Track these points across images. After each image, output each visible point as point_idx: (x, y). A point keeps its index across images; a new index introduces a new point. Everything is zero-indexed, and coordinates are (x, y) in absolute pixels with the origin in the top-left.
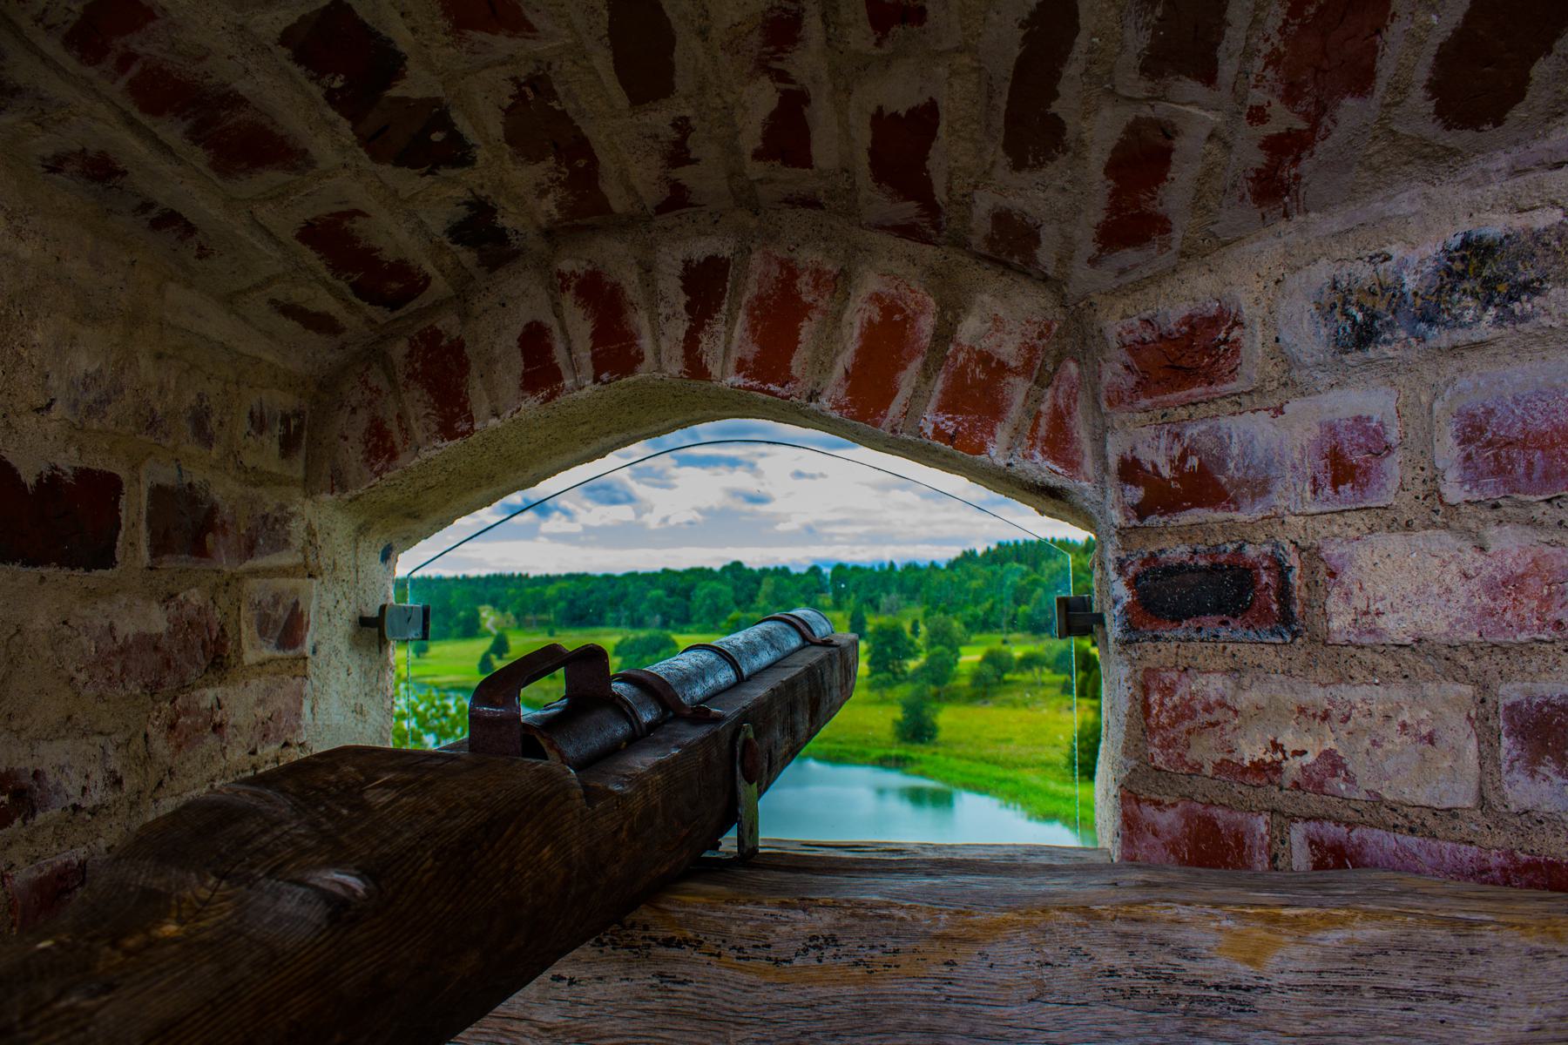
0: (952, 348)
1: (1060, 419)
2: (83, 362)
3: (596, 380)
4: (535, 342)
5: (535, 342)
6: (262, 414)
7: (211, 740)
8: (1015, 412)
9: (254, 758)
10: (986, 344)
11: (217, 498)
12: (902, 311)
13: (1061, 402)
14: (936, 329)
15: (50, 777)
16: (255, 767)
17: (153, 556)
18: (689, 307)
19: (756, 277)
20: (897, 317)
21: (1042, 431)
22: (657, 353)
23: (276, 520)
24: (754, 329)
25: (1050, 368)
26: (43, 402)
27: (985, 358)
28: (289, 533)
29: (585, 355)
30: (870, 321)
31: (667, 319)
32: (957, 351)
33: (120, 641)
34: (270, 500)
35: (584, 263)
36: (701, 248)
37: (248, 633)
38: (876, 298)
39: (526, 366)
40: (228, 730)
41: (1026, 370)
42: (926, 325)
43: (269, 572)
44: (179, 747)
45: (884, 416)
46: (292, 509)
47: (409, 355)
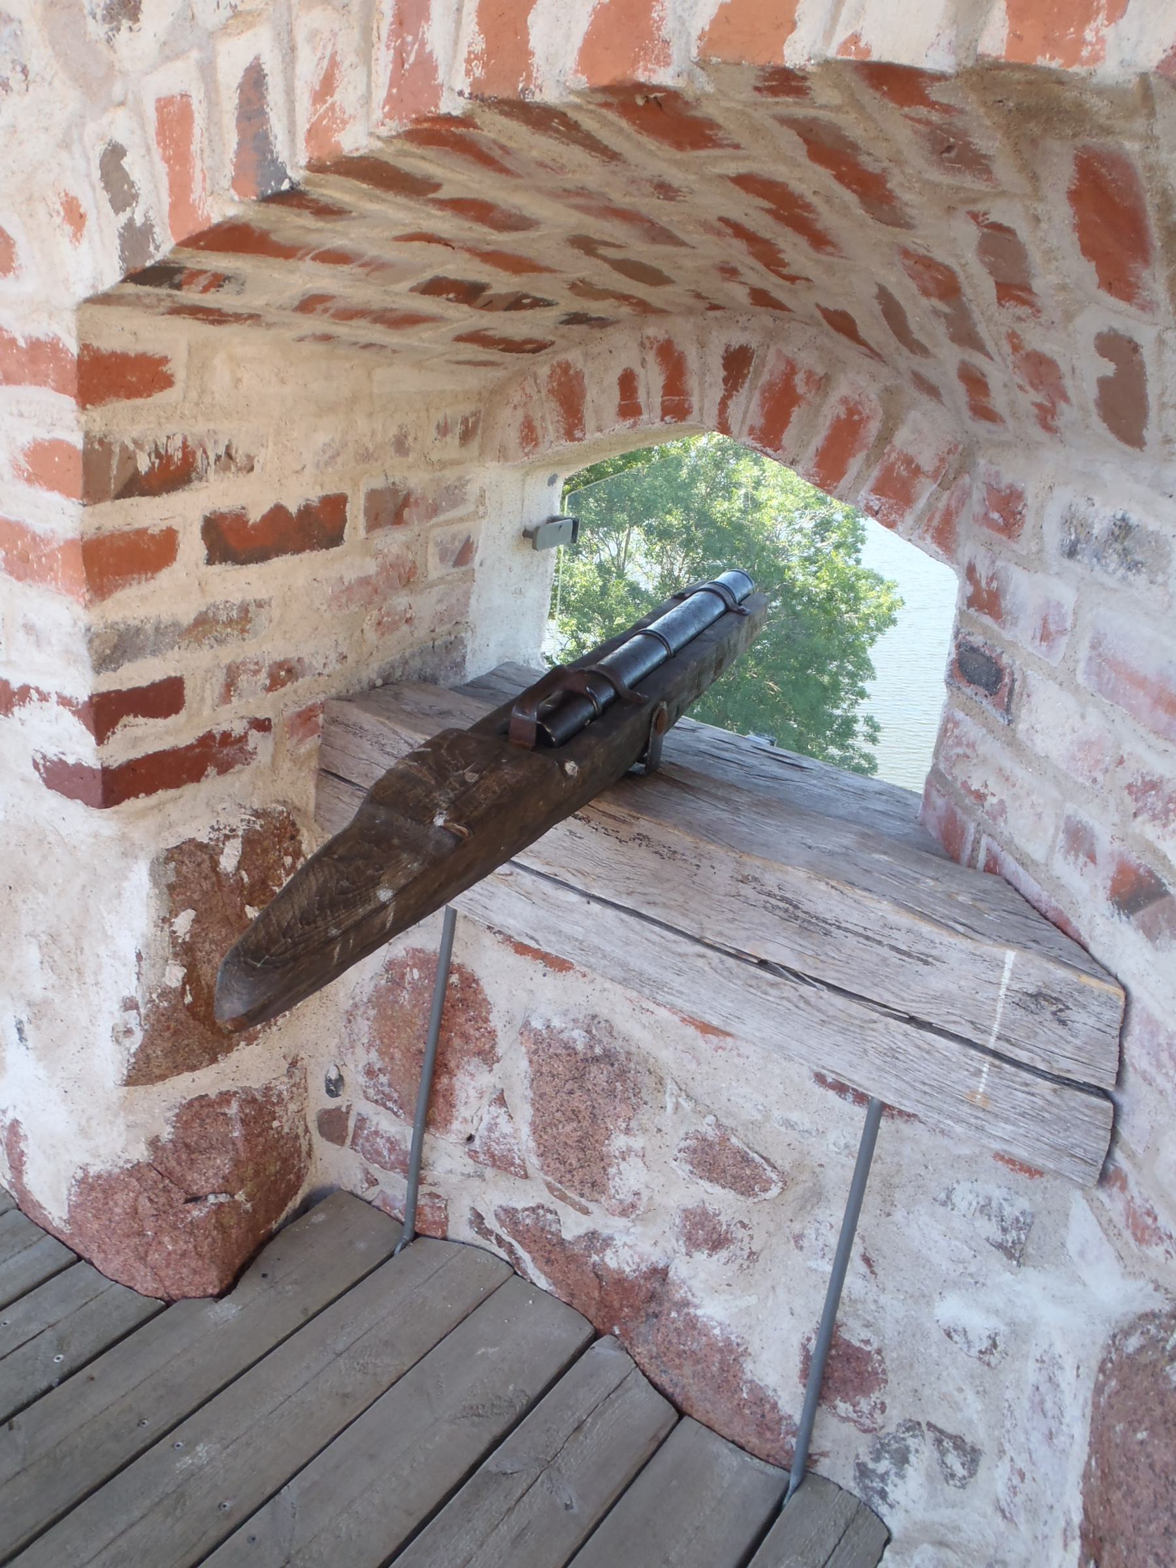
0: (888, 447)
1: (949, 516)
2: (322, 438)
3: (662, 420)
4: (627, 382)
5: (627, 382)
6: (446, 423)
7: (405, 628)
8: (921, 503)
9: (433, 635)
10: (911, 451)
11: (412, 485)
12: (860, 413)
13: (953, 503)
14: (880, 432)
15: (306, 660)
16: (434, 640)
17: (368, 532)
18: (725, 380)
19: (767, 370)
20: (856, 417)
21: (935, 523)
22: (701, 409)
23: (456, 487)
24: (762, 406)
25: (951, 477)
26: (299, 468)
27: (908, 461)
28: (465, 494)
29: (657, 400)
30: (838, 417)
31: (710, 386)
32: (892, 450)
33: (346, 584)
34: (450, 475)
35: (663, 332)
36: (737, 339)
37: (433, 561)
38: (844, 401)
39: (622, 399)
40: (416, 621)
41: (935, 475)
42: (873, 428)
43: (449, 523)
44: (383, 634)
45: (836, 488)
46: (468, 477)
47: (551, 376)
